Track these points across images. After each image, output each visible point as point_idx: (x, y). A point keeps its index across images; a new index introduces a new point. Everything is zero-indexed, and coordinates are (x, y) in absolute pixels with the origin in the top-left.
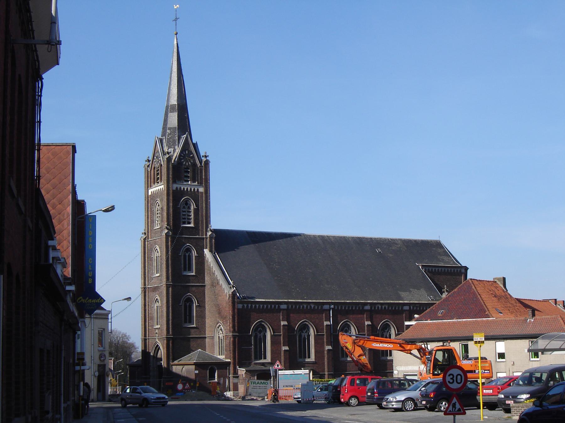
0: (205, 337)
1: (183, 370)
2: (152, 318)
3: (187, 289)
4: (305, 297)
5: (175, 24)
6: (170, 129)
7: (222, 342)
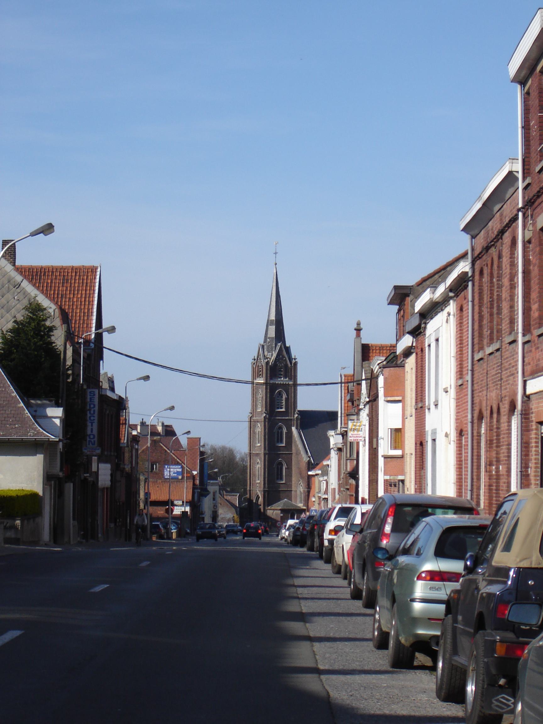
0: (292, 491)
2: (255, 475)
3: (279, 455)
6: (269, 338)
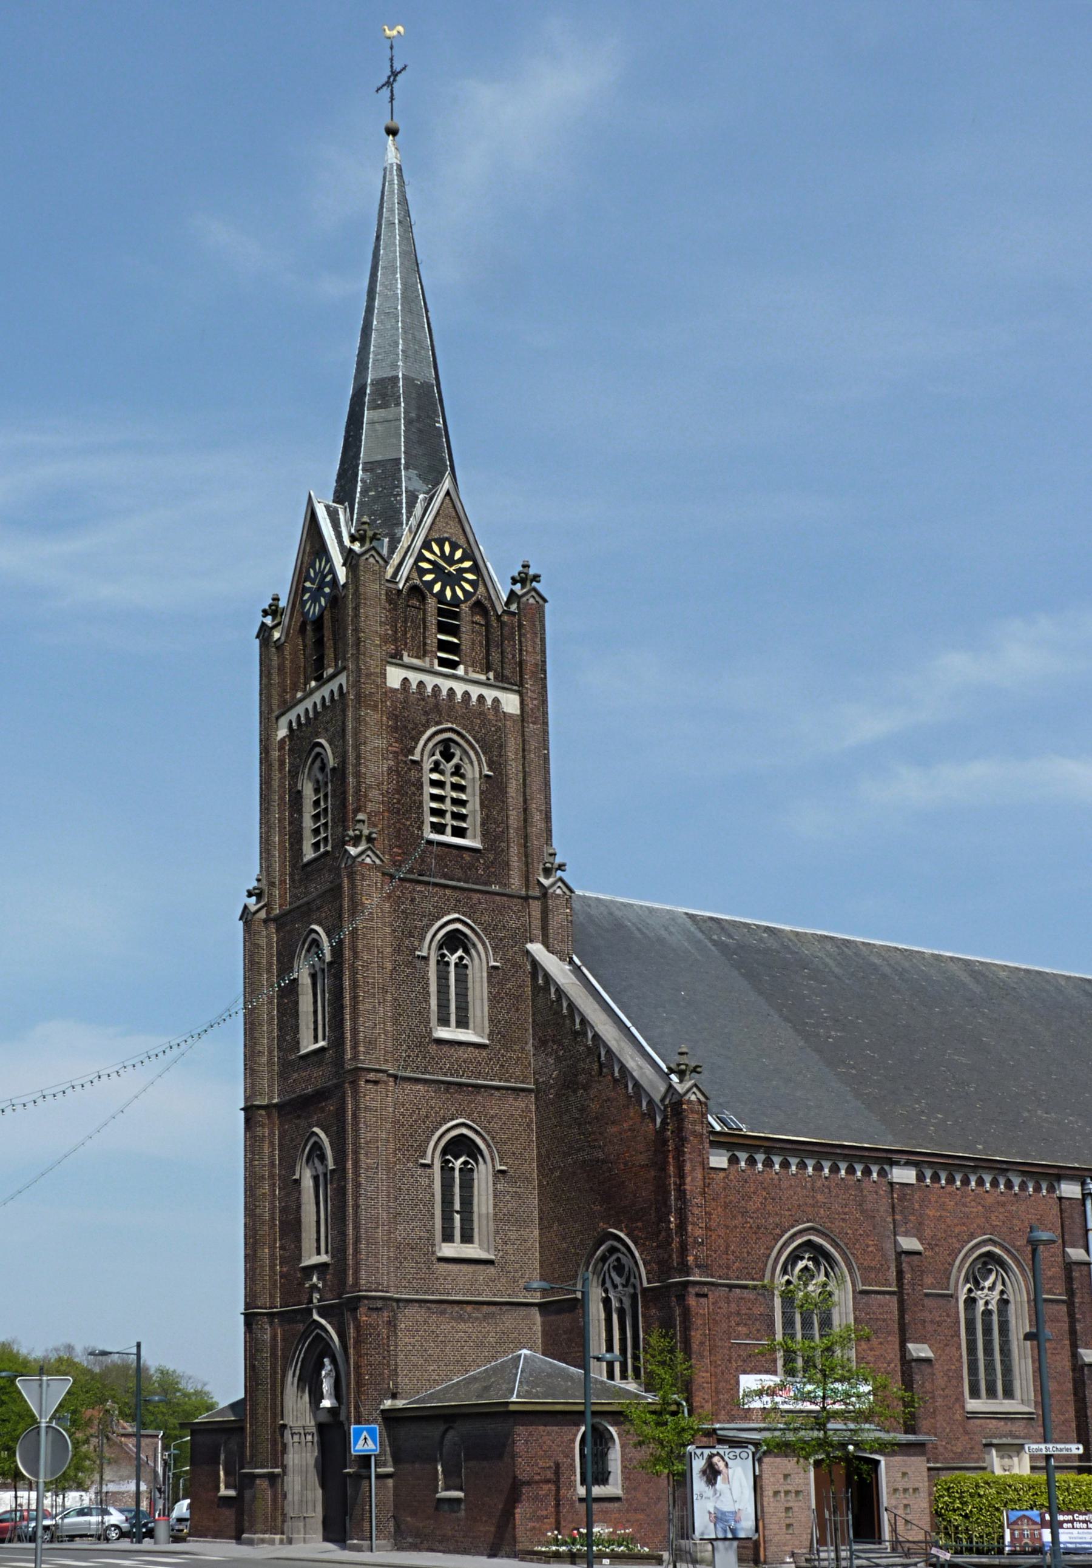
1: (446, 1442)
4: (980, 1147)
5: (390, 94)
7: (987, 1331)
